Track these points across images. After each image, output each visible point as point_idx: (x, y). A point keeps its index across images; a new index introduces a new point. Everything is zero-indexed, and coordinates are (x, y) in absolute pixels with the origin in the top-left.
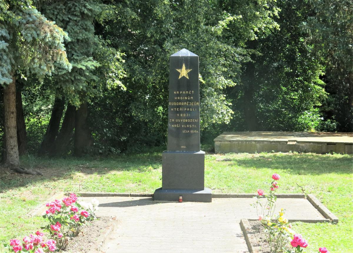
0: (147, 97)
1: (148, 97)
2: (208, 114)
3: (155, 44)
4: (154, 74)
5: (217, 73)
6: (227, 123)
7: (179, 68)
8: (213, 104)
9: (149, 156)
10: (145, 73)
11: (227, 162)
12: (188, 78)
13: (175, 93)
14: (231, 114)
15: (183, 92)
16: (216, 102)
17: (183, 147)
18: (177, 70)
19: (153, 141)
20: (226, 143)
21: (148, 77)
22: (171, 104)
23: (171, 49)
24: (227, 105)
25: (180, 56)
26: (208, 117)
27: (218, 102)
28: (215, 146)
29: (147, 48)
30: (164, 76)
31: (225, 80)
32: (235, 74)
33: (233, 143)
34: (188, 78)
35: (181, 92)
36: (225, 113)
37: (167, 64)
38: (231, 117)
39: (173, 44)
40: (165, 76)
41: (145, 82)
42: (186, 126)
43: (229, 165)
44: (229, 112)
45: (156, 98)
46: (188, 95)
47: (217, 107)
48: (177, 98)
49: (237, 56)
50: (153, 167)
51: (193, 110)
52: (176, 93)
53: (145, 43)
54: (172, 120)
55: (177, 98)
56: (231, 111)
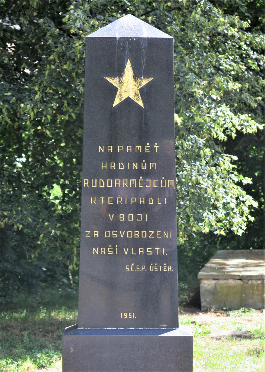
0: (20, 162)
1: (23, 163)
2: (187, 210)
3: (40, 16)
4: (37, 97)
5: (210, 98)
6: (240, 233)
7: (113, 76)
8: (201, 182)
9: (25, 320)
10: (13, 96)
11: (244, 341)
12: (141, 103)
13: (101, 149)
14: (251, 207)
15: (125, 148)
16: (210, 176)
17: (126, 315)
18: (108, 79)
19: (37, 274)
20: (231, 282)
21: (22, 105)
22: (90, 184)
23: (86, 26)
24: (239, 184)
25: (118, 36)
26: (188, 217)
27: (215, 176)
28: (202, 291)
29: (18, 27)
30: (66, 104)
31: (232, 114)
32: (256, 101)
33: (250, 282)
34: (141, 103)
35: (120, 148)
36: (233, 205)
37: (73, 70)
38: (250, 217)
39: (92, 14)
40: (68, 104)
41: (13, 121)
42: (136, 251)
43: (249, 353)
44: (243, 202)
45: (43, 163)
46: (141, 157)
47: (214, 190)
48: (109, 166)
49: (254, 57)
50: (35, 361)
51: (155, 201)
52: (106, 149)
53: (14, 12)
54: (91, 235)
55: (109, 166)
56: (250, 200)
